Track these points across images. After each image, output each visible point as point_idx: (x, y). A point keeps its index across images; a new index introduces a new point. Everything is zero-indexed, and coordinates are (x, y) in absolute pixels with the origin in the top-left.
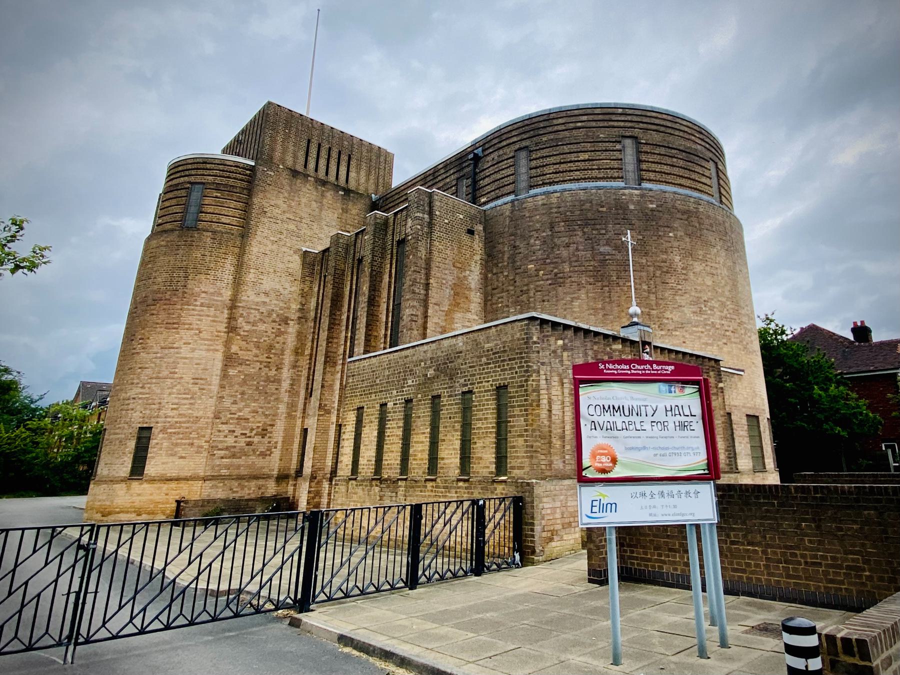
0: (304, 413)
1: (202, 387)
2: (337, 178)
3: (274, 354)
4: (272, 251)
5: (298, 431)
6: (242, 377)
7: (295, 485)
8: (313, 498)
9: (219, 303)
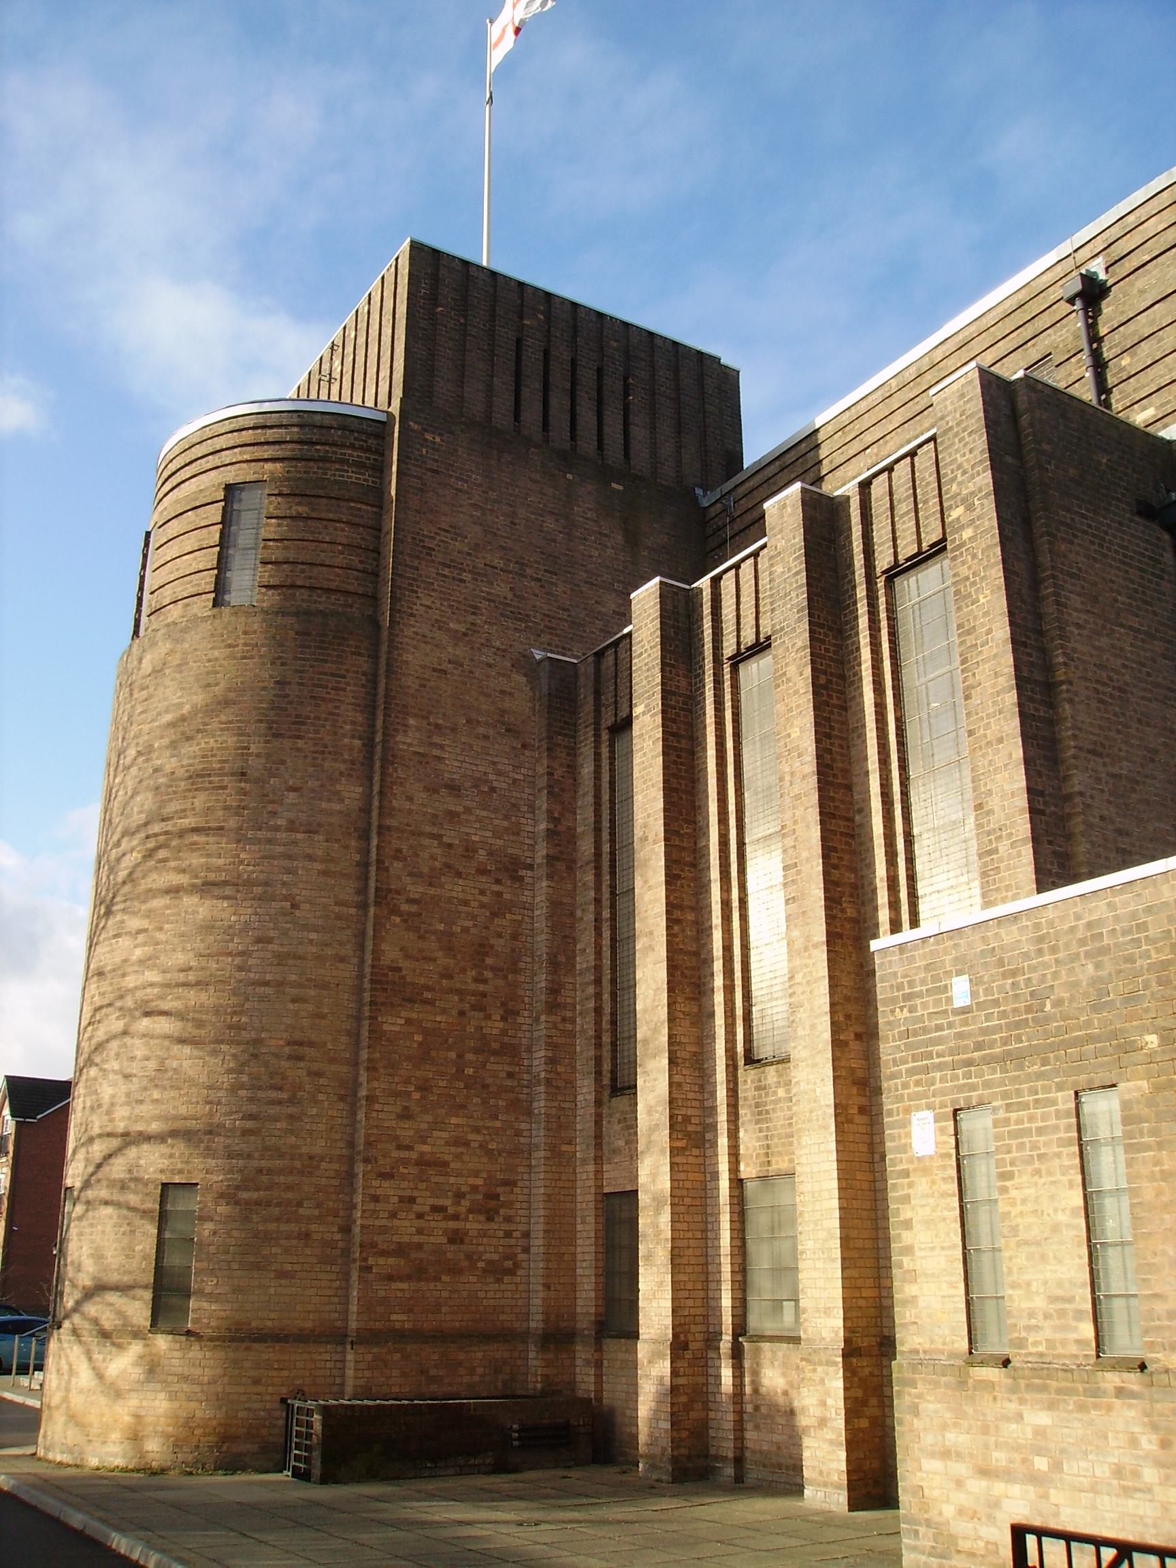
0: (598, 1146)
1: (316, 1067)
2: (600, 447)
3: (492, 969)
4: (457, 663)
5: (585, 1202)
6: (418, 1038)
7: (599, 1364)
8: (688, 1408)
9: (335, 820)
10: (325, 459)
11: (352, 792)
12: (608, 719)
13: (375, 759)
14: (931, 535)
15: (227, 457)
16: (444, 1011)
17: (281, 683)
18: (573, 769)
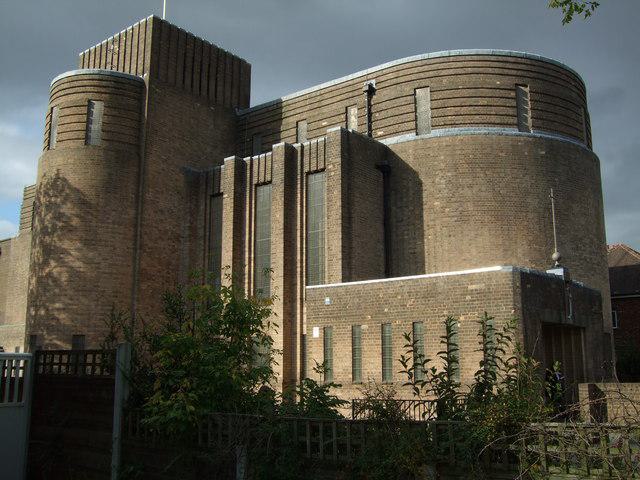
10: (123, 95)
11: (132, 212)
12: (210, 192)
13: (139, 200)
14: (321, 166)
15: (88, 89)
16: (157, 283)
17: (110, 174)
18: (197, 206)
